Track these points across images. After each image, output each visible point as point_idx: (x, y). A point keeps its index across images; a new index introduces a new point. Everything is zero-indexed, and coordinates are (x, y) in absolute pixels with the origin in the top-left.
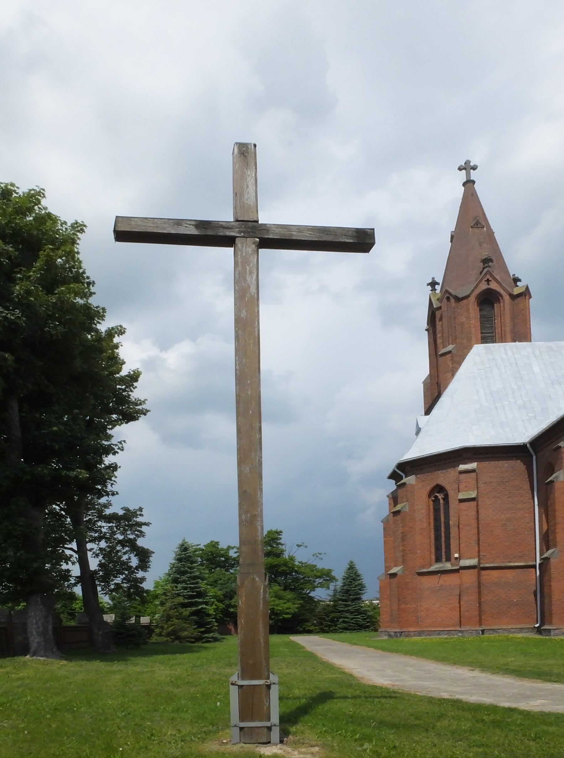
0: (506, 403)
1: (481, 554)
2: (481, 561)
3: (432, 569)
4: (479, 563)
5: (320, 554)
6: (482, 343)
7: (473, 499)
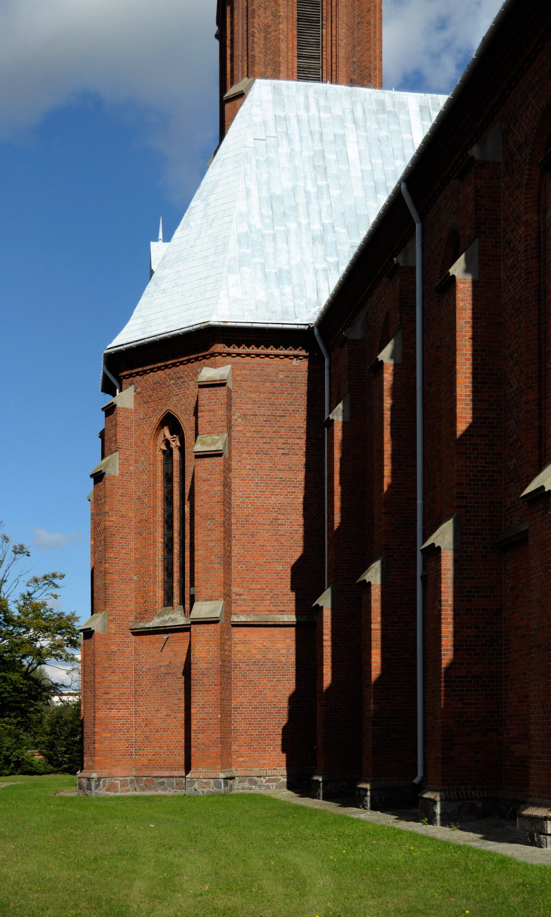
0: (292, 225)
1: (235, 589)
2: (234, 608)
3: (156, 622)
4: (228, 611)
5: (54, 576)
6: (300, 78)
7: (218, 454)
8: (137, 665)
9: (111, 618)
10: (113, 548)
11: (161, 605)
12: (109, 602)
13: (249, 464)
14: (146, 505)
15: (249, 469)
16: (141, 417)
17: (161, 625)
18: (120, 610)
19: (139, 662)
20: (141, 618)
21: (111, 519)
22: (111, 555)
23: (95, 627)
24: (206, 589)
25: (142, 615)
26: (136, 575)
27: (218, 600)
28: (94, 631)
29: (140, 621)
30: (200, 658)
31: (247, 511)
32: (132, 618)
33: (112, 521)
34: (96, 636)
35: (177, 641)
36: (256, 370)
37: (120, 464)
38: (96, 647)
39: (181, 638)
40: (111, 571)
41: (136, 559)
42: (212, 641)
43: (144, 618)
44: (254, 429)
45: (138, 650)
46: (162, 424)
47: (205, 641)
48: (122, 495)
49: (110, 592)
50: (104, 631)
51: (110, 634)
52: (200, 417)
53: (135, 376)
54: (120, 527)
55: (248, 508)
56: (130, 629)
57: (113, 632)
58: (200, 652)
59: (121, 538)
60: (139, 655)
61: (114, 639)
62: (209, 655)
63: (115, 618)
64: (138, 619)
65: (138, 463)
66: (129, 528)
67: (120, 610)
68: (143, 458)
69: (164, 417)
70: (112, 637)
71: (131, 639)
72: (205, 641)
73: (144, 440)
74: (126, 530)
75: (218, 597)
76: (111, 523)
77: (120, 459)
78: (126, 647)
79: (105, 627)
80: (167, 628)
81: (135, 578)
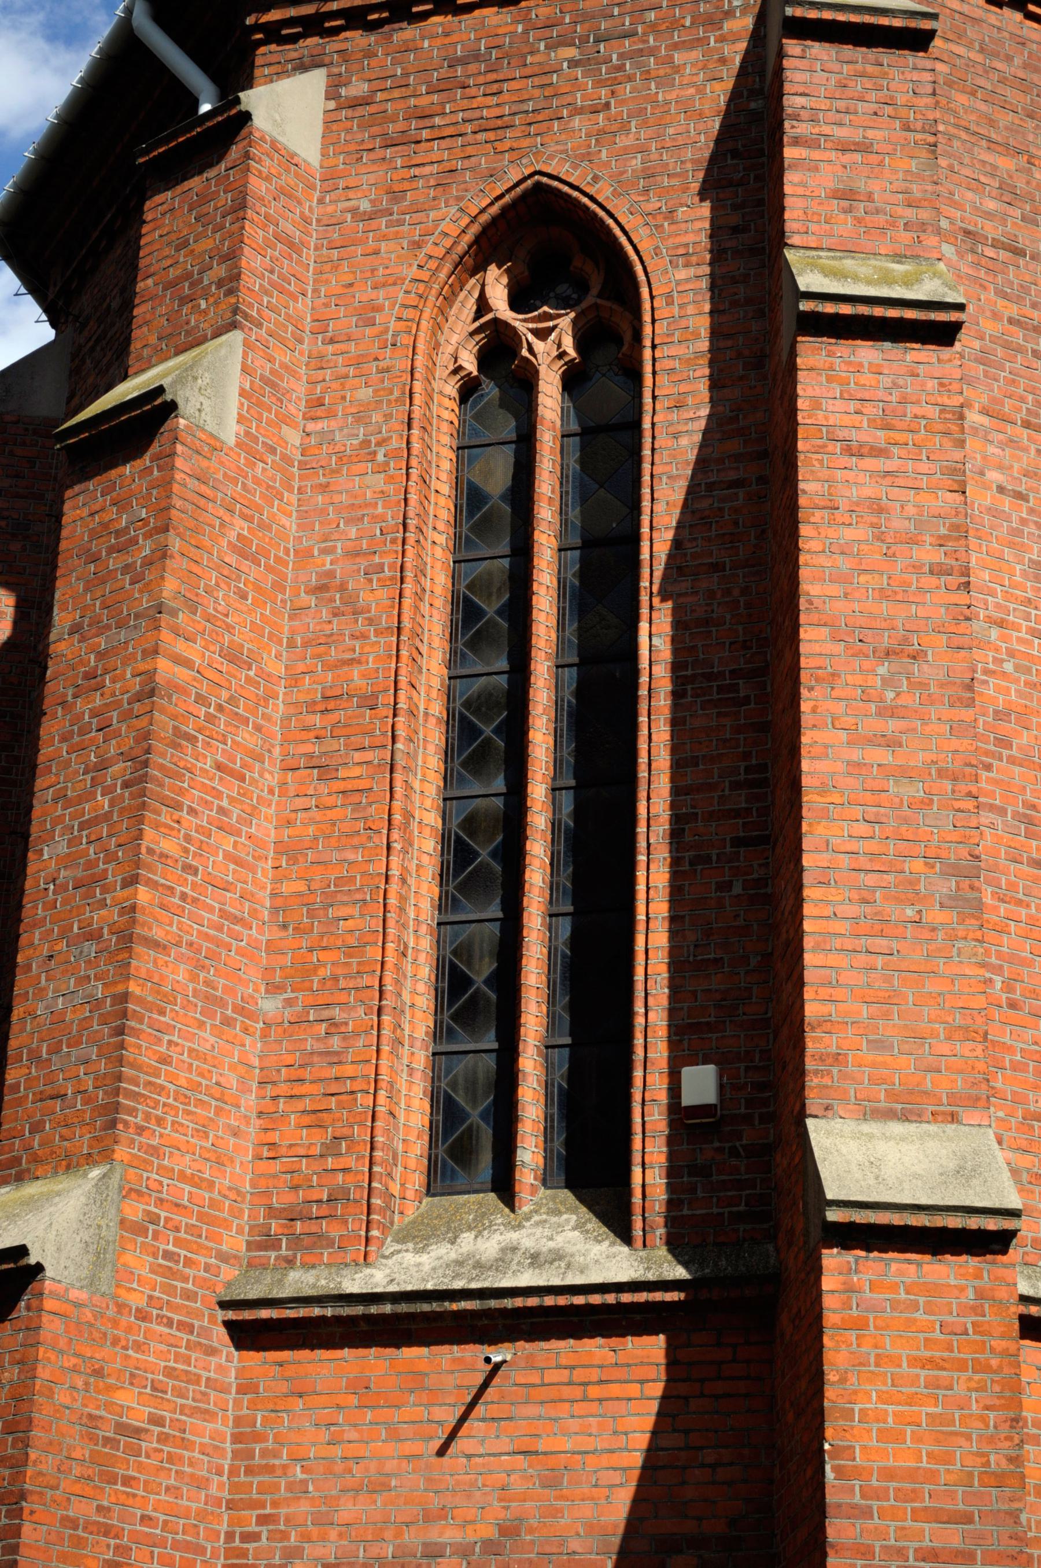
8: (247, 1537)
9: (135, 1210)
10: (178, 806)
11: (417, 1180)
12: (133, 1112)
13: (1000, 467)
14: (370, 621)
15: (1001, 489)
16: (365, 205)
17: (458, 1284)
18: (183, 1177)
19: (263, 1520)
20: (296, 1242)
21: (181, 647)
22: (168, 845)
23: (50, 1248)
24: (878, 1045)
25: (294, 1225)
26: (274, 989)
27: (953, 1118)
28: (39, 1268)
29: (290, 1262)
30: (888, 1474)
31: (998, 689)
32: (235, 1241)
33: (187, 664)
34: (49, 1304)
35: (567, 1392)
36: (1009, 59)
37: (242, 393)
38: (44, 1373)
39: (595, 1375)
40: (157, 933)
41: (280, 906)
42: (961, 1366)
43: (320, 1240)
44: (1013, 310)
45: (258, 1437)
46: (487, 246)
47: (913, 1362)
48: (242, 547)
49: (141, 1049)
50: (92, 1281)
51: (121, 1307)
52: (794, 166)
53: (336, 31)
54: (220, 708)
55: (1004, 675)
56: (224, 1305)
57: (136, 1301)
58: (884, 1435)
59: (219, 767)
60: (270, 1469)
61: (138, 1346)
62: (947, 1459)
63: (154, 1219)
64: (276, 1245)
65: (331, 415)
66: (258, 728)
67: (183, 1177)
68: (365, 394)
69: (505, 210)
70: (129, 1329)
71: (220, 1368)
72: (913, 1362)
73: (379, 309)
74: (246, 736)
75: (954, 1099)
76: (181, 674)
77: (245, 369)
78: (194, 1412)
79: (98, 1263)
80: (509, 1303)
81: (270, 1006)
